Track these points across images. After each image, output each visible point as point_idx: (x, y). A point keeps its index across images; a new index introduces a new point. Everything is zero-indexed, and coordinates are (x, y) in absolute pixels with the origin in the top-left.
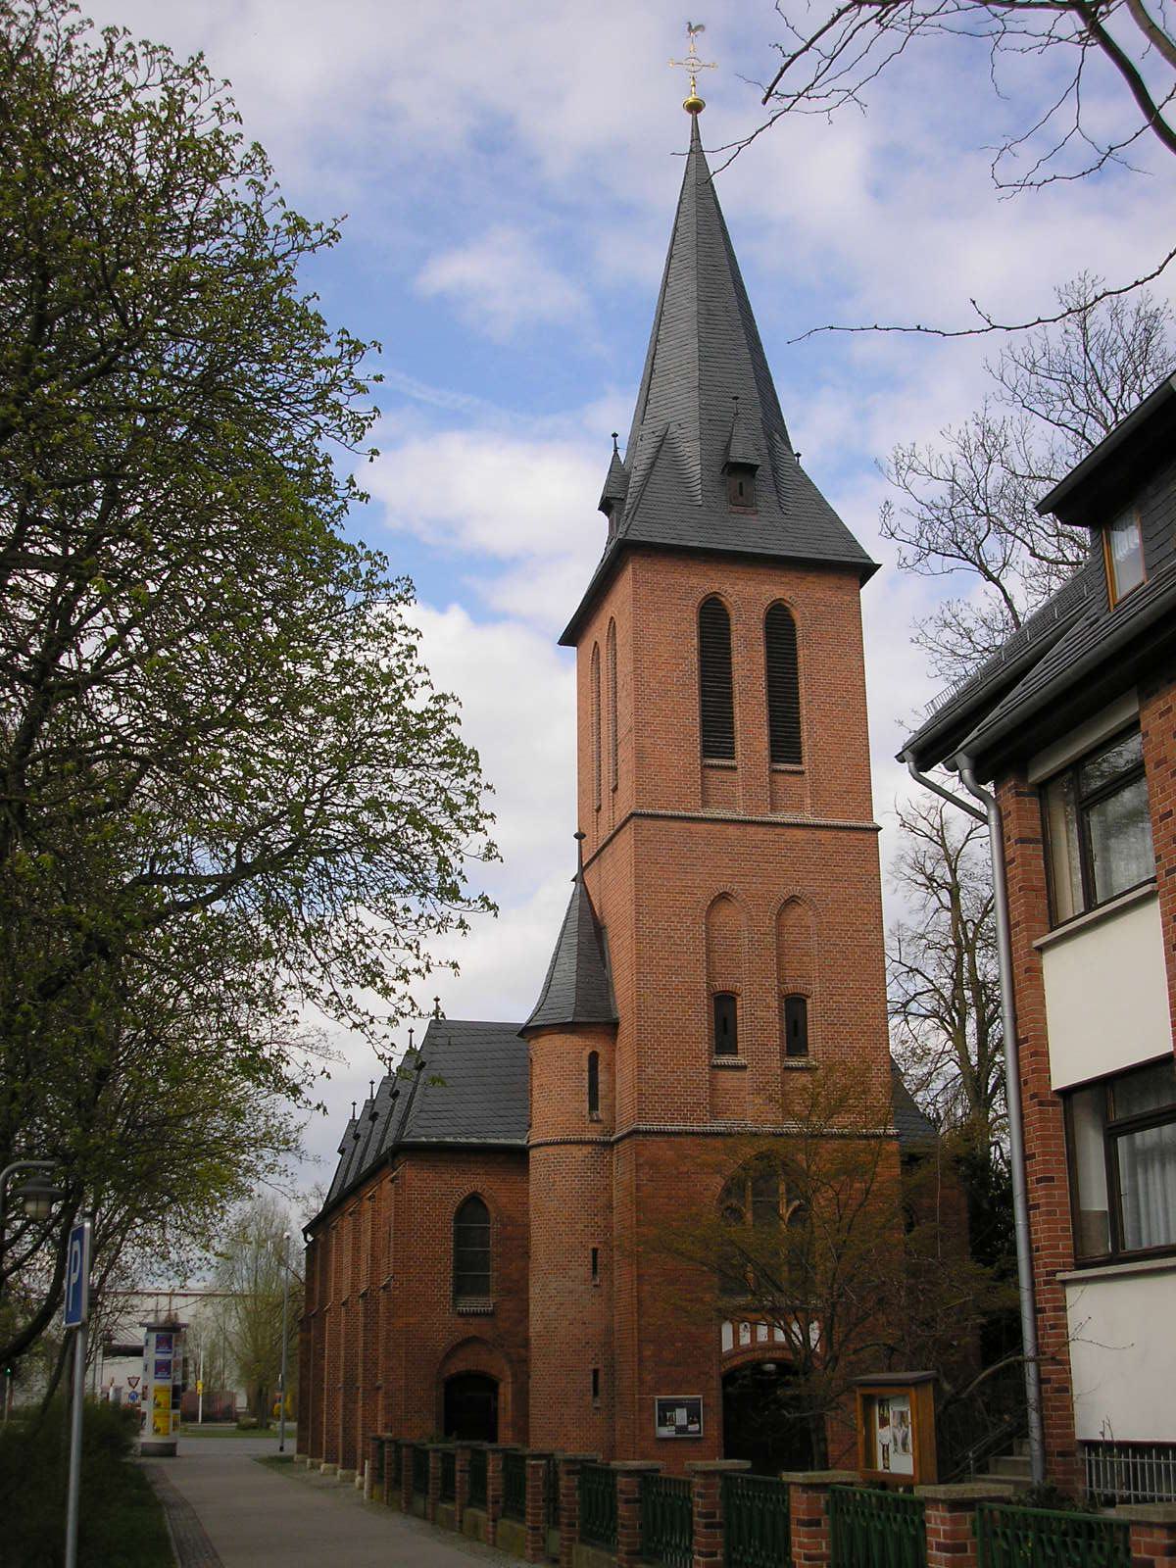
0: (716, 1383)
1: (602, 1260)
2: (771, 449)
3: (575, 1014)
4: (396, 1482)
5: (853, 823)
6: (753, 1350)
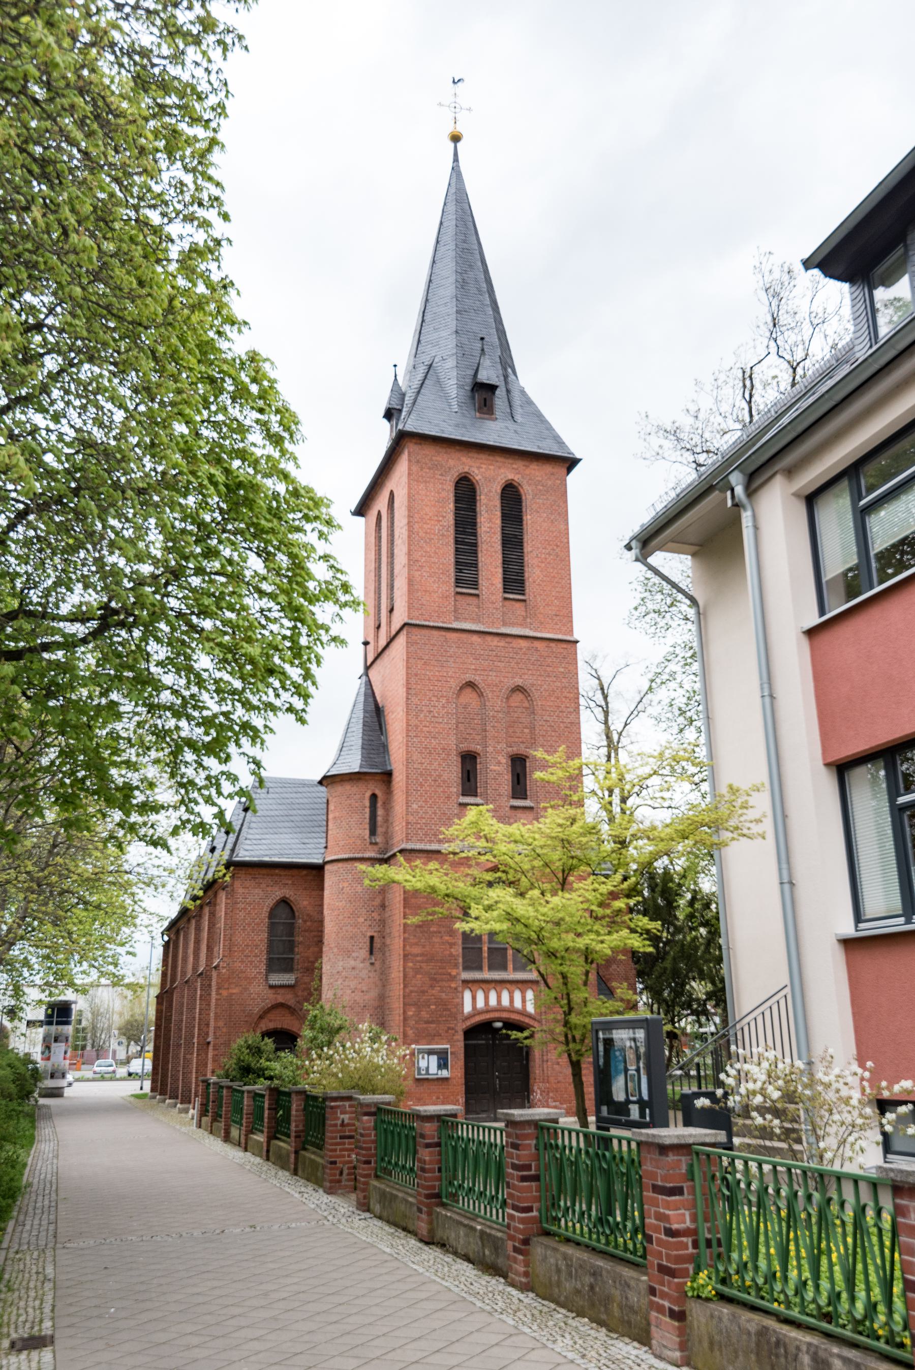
0: (460, 1036)
1: (377, 943)
2: (506, 377)
3: (361, 767)
4: (216, 1118)
5: (560, 637)
6: (487, 1011)
